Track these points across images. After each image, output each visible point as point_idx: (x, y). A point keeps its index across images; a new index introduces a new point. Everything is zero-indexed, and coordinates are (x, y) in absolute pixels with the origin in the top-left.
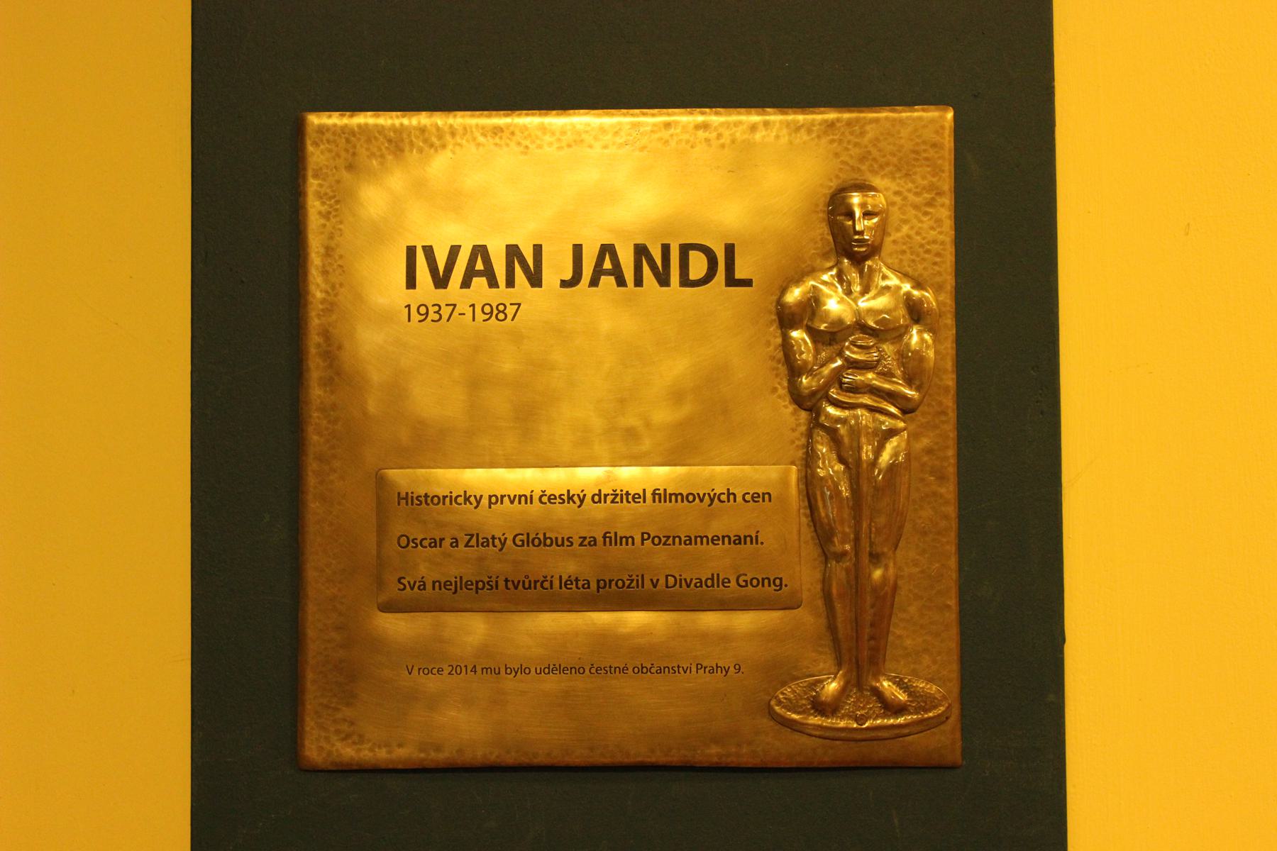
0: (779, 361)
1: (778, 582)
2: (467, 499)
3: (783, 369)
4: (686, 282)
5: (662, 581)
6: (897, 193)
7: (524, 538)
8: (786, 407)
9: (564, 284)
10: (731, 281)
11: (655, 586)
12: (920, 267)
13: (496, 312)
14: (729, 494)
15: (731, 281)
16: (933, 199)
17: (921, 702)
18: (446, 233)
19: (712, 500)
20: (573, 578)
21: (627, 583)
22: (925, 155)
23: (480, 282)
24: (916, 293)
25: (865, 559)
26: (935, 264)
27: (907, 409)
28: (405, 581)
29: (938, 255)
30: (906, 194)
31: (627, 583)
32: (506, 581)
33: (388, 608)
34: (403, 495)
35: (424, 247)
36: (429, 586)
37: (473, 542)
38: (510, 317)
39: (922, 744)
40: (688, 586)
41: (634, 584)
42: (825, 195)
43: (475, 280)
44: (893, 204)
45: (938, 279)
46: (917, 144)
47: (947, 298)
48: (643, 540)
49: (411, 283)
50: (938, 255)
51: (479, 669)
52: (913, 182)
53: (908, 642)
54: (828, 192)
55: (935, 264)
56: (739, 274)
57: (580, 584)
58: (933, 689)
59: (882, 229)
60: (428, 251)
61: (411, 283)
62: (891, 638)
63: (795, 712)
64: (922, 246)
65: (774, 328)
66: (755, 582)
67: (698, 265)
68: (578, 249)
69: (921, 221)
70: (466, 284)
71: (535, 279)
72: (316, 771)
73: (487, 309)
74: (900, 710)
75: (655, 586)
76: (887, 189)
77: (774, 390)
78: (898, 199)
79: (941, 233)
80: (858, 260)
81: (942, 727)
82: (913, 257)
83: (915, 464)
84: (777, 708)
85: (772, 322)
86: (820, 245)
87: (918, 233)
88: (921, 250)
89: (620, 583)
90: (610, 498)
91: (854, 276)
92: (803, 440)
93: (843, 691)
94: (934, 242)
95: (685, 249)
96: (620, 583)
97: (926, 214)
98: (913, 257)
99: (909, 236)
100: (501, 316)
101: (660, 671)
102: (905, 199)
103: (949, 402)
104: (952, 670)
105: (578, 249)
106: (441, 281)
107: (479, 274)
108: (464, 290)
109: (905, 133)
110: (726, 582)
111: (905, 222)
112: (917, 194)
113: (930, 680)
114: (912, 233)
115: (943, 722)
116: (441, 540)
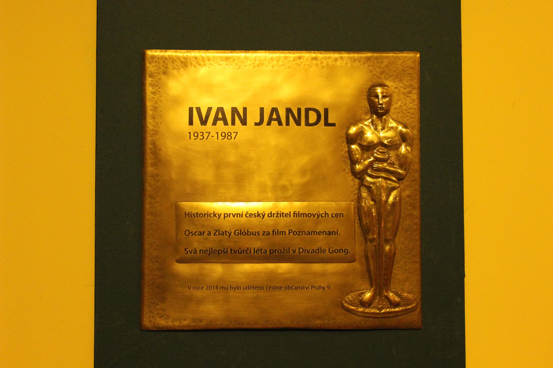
0: (346, 158)
1: (346, 251)
3: (348, 162)
4: (307, 124)
5: (297, 251)
6: (396, 88)
7: (239, 232)
9: (256, 124)
11: (294, 252)
19: (318, 216)
20: (260, 249)
21: (283, 251)
23: (220, 123)
30: (400, 88)
31: (283, 251)
32: (231, 250)
34: (187, 213)
37: (217, 233)
38: (233, 138)
40: (308, 252)
47: (416, 132)
48: (289, 233)
52: (403, 83)
55: (412, 118)
56: (330, 122)
57: (263, 251)
58: (410, 296)
59: (389, 104)
60: (198, 110)
62: (393, 275)
64: (406, 110)
65: (345, 144)
67: (313, 117)
68: (262, 110)
70: (214, 123)
71: (244, 122)
72: (148, 331)
74: (397, 305)
75: (294, 252)
80: (380, 116)
83: (403, 202)
84: (345, 304)
87: (405, 105)
89: (280, 251)
90: (275, 215)
95: (307, 110)
100: (229, 137)
104: (417, 289)
105: (262, 110)
107: (220, 119)
110: (324, 251)
112: (404, 89)
116: (204, 232)
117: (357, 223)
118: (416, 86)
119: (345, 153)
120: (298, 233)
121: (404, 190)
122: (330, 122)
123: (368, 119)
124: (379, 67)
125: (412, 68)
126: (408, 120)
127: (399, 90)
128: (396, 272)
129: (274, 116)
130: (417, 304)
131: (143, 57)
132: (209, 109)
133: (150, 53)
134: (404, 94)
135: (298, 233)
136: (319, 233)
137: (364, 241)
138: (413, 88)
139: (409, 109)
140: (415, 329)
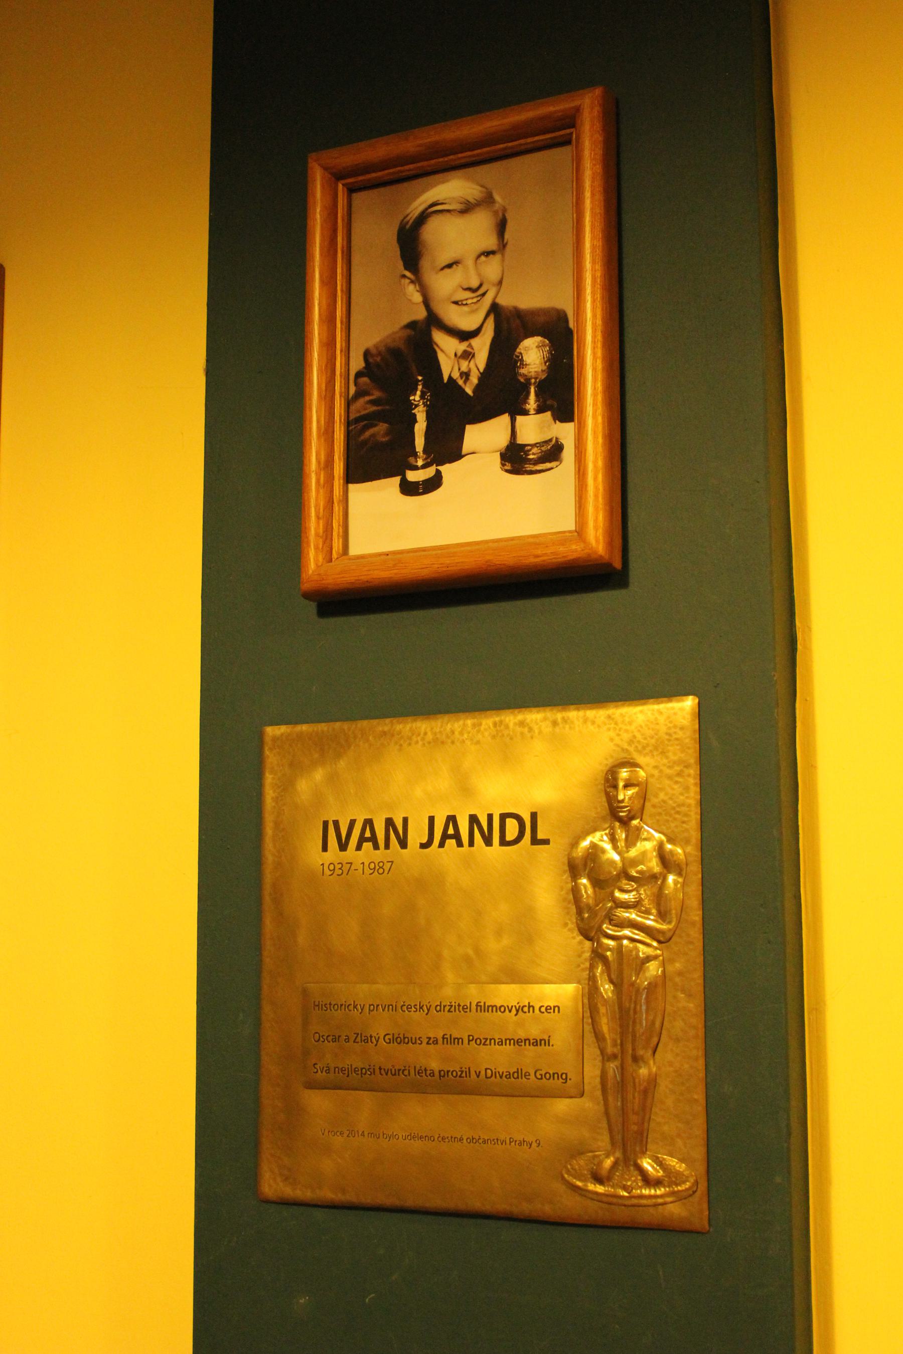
0: (569, 902)
1: (564, 1076)
2: (355, 1007)
3: (573, 909)
4: (503, 842)
5: (483, 1073)
6: (656, 767)
7: (390, 1037)
8: (574, 938)
9: (424, 846)
10: (535, 841)
11: (478, 1076)
12: (673, 825)
13: (377, 868)
14: (529, 1007)
15: (535, 841)
16: (682, 771)
17: (671, 1177)
18: (350, 812)
19: (517, 1011)
20: (423, 1068)
21: (459, 1073)
22: (675, 736)
23: (367, 846)
24: (669, 847)
25: (629, 1059)
26: (683, 822)
27: (662, 939)
28: (317, 1067)
29: (686, 815)
30: (662, 768)
31: (459, 1073)
32: (380, 1069)
33: (311, 1085)
34: (317, 1003)
35: (333, 821)
36: (332, 1070)
37: (359, 1039)
38: (386, 872)
39: (675, 1210)
40: (501, 1077)
41: (464, 1074)
42: (602, 771)
43: (448, 841)
44: (653, 776)
45: (686, 835)
46: (669, 728)
47: (693, 849)
48: (469, 1041)
49: (325, 848)
50: (686, 815)
51: (366, 1133)
52: (667, 758)
53: (666, 1128)
54: (605, 769)
55: (683, 822)
56: (540, 836)
57: (428, 1072)
58: (681, 1167)
59: (643, 797)
60: (336, 824)
61: (325, 848)
62: (652, 1125)
63: (580, 1180)
64: (674, 808)
65: (566, 876)
66: (548, 1076)
67: (512, 828)
68: (432, 820)
69: (673, 789)
70: (359, 848)
71: (403, 844)
72: (267, 1201)
73: (372, 866)
74: (657, 1183)
75: (478, 1076)
76: (648, 765)
77: (566, 925)
78: (656, 772)
79: (687, 798)
80: (625, 823)
81: (691, 1199)
82: (668, 818)
83: (669, 984)
84: (566, 1176)
85: (565, 872)
86: (599, 810)
87: (671, 799)
88: (673, 812)
89: (454, 1074)
90: (447, 1008)
91: (621, 835)
92: (587, 964)
93: (615, 1164)
94: (683, 805)
95: (503, 817)
96: (454, 1074)
97: (677, 782)
98: (668, 818)
99: (664, 801)
100: (381, 871)
101: (485, 1142)
102: (661, 771)
103: (696, 933)
104: (699, 1153)
105: (432, 820)
106: (343, 847)
107: (367, 840)
108: (441, 849)
109: (662, 719)
110: (527, 1075)
111: (661, 789)
112: (670, 767)
113: (681, 1160)
114: (666, 798)
115: (691, 1195)
116: (339, 1036)
117: (588, 1024)
118: (692, 761)
119: (567, 893)
120: (483, 1041)
121: (672, 961)
122: (540, 836)
123: (605, 830)
124: (626, 731)
125: (682, 728)
126: (676, 826)
127: (661, 771)
128: (659, 1120)
129: (451, 831)
130: (696, 1183)
131: (261, 735)
132: (352, 823)
133: (271, 731)
134: (670, 777)
135: (483, 1041)
136: (501, 1043)
137: (601, 1058)
138: (687, 767)
139: (679, 806)
140: (676, 1231)
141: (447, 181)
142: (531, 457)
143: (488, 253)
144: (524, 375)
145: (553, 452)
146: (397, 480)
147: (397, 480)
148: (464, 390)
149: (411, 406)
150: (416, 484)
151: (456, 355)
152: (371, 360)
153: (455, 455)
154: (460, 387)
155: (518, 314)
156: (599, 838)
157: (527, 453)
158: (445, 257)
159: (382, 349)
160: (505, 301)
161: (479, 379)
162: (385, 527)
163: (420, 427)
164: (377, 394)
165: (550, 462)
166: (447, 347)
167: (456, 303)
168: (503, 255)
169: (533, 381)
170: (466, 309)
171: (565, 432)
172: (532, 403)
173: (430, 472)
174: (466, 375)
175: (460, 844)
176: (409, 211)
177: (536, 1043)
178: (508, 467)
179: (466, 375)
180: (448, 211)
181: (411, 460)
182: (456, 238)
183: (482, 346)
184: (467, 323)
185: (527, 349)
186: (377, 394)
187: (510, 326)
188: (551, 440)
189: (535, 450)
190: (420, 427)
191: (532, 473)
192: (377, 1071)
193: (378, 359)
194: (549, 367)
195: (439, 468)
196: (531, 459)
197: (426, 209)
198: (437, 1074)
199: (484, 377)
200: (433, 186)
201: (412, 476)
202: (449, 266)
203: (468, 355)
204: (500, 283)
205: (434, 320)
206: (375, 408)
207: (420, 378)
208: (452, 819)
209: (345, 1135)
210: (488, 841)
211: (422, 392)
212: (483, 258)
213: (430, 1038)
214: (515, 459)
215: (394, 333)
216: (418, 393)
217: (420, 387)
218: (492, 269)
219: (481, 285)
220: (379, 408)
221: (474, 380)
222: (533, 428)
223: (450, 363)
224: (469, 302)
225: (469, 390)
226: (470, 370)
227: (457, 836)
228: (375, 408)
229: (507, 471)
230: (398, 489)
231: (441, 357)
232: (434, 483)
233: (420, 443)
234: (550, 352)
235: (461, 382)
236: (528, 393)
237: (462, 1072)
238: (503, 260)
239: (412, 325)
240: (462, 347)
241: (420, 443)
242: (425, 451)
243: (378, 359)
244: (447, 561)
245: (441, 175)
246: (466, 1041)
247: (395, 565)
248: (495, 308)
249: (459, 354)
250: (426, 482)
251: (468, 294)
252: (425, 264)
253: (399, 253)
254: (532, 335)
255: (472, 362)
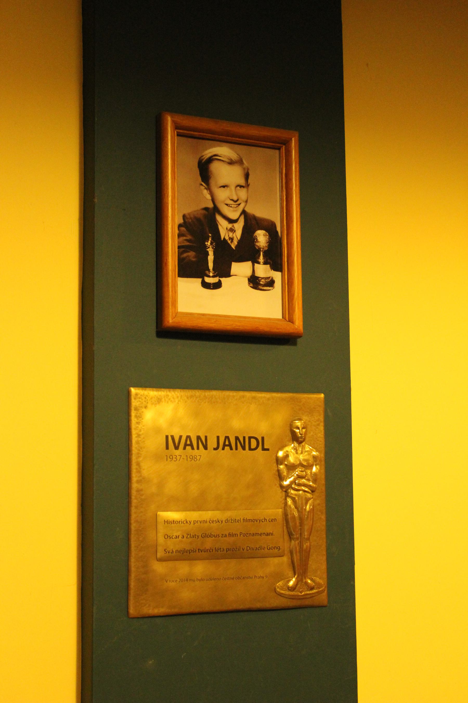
4: (250, 449)
5: (246, 549)
9: (215, 449)
10: (264, 449)
11: (243, 550)
15: (264, 449)
23: (188, 448)
32: (199, 550)
58: (321, 582)
68: (218, 437)
70: (184, 448)
71: (206, 448)
75: (243, 550)
77: (276, 485)
90: (230, 521)
95: (250, 438)
100: (195, 460)
105: (218, 437)
112: (315, 422)
122: (265, 447)
129: (227, 443)
134: (314, 426)
141: (222, 146)
142: (261, 283)
143: (241, 186)
144: (258, 246)
145: (271, 283)
146: (200, 280)
147: (200, 280)
148: (230, 246)
149: (206, 247)
150: (210, 284)
151: (227, 229)
152: (186, 220)
153: (228, 275)
154: (229, 244)
155: (254, 218)
156: (290, 448)
157: (260, 281)
158: (222, 183)
159: (192, 216)
160: (248, 210)
161: (238, 243)
162: (191, 300)
163: (211, 258)
164: (189, 237)
165: (270, 287)
166: (223, 225)
167: (227, 205)
168: (248, 188)
169: (262, 250)
170: (231, 208)
171: (277, 276)
172: (261, 259)
173: (216, 280)
174: (232, 239)
175: (231, 449)
176: (203, 154)
177: (268, 534)
178: (251, 285)
179: (232, 239)
180: (223, 161)
181: (207, 272)
182: (226, 174)
183: (239, 227)
184: (234, 215)
185: (259, 235)
186: (189, 237)
187: (252, 224)
188: (269, 277)
189: (263, 280)
190: (211, 258)
191: (261, 290)
192: (197, 551)
193: (190, 221)
194: (269, 245)
195: (221, 279)
196: (261, 284)
197: (212, 156)
198: (225, 550)
199: (240, 242)
200: (215, 146)
201: (207, 280)
202: (224, 187)
203: (232, 230)
204: (246, 202)
205: (216, 210)
206: (188, 244)
207: (210, 235)
208: (227, 438)
209: (178, 582)
210: (244, 448)
211: (211, 241)
212: (238, 188)
213: (223, 535)
214: (254, 282)
215: (197, 210)
216: (209, 242)
217: (210, 239)
218: (243, 194)
219: (238, 200)
220: (191, 244)
221: (235, 242)
222: (263, 270)
223: (224, 232)
224: (233, 206)
225: (233, 246)
226: (233, 237)
227: (230, 445)
228: (188, 244)
229: (251, 287)
230: (200, 284)
231: (220, 228)
232: (218, 286)
233: (211, 265)
234: (269, 239)
235: (229, 242)
236: (260, 255)
237: (237, 548)
238: (248, 190)
239: (206, 209)
240: (230, 226)
241: (211, 265)
242: (213, 269)
243: (190, 221)
244: (238, 324)
245: (218, 143)
246: (239, 535)
247: (215, 322)
248: (244, 212)
249: (228, 228)
250: (214, 284)
251: (232, 202)
252: (212, 182)
253: (199, 173)
254: (261, 229)
255: (234, 234)
